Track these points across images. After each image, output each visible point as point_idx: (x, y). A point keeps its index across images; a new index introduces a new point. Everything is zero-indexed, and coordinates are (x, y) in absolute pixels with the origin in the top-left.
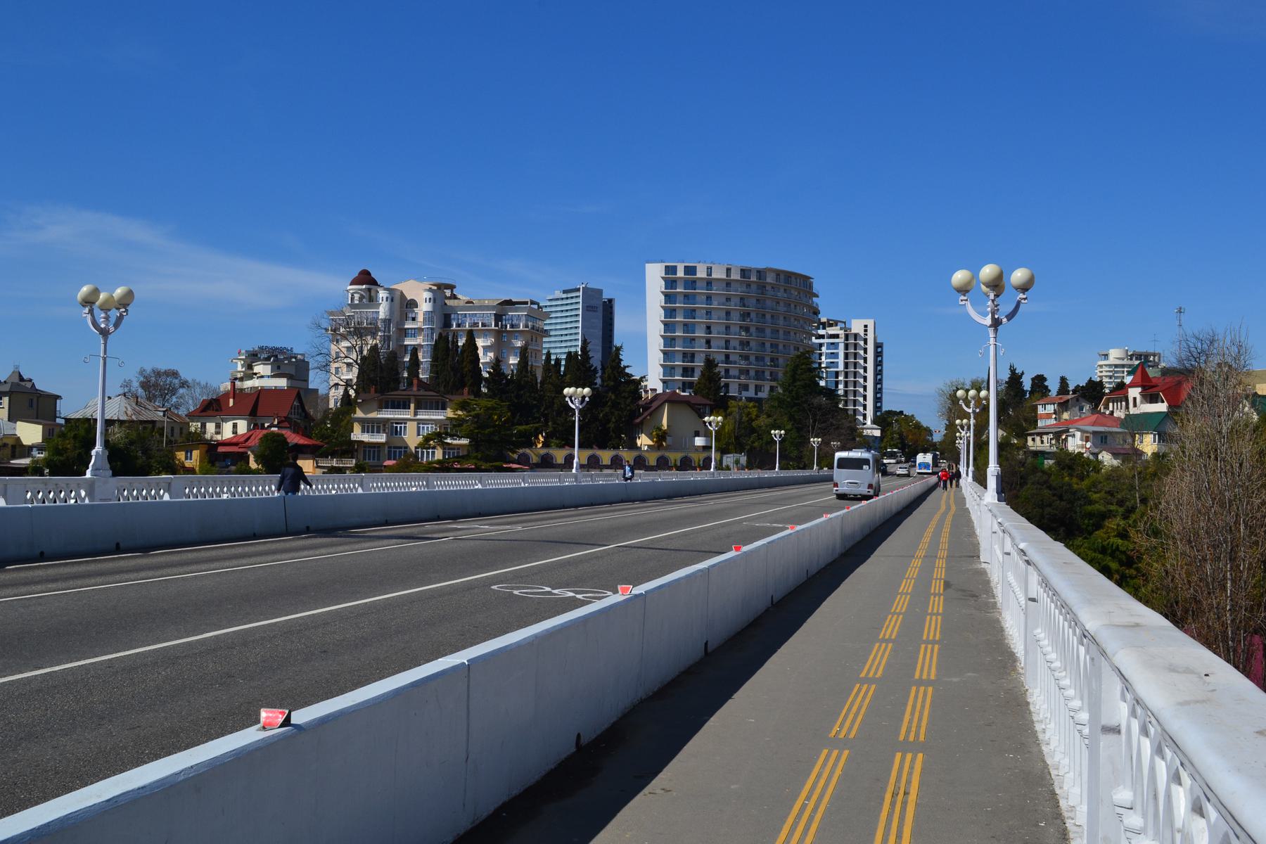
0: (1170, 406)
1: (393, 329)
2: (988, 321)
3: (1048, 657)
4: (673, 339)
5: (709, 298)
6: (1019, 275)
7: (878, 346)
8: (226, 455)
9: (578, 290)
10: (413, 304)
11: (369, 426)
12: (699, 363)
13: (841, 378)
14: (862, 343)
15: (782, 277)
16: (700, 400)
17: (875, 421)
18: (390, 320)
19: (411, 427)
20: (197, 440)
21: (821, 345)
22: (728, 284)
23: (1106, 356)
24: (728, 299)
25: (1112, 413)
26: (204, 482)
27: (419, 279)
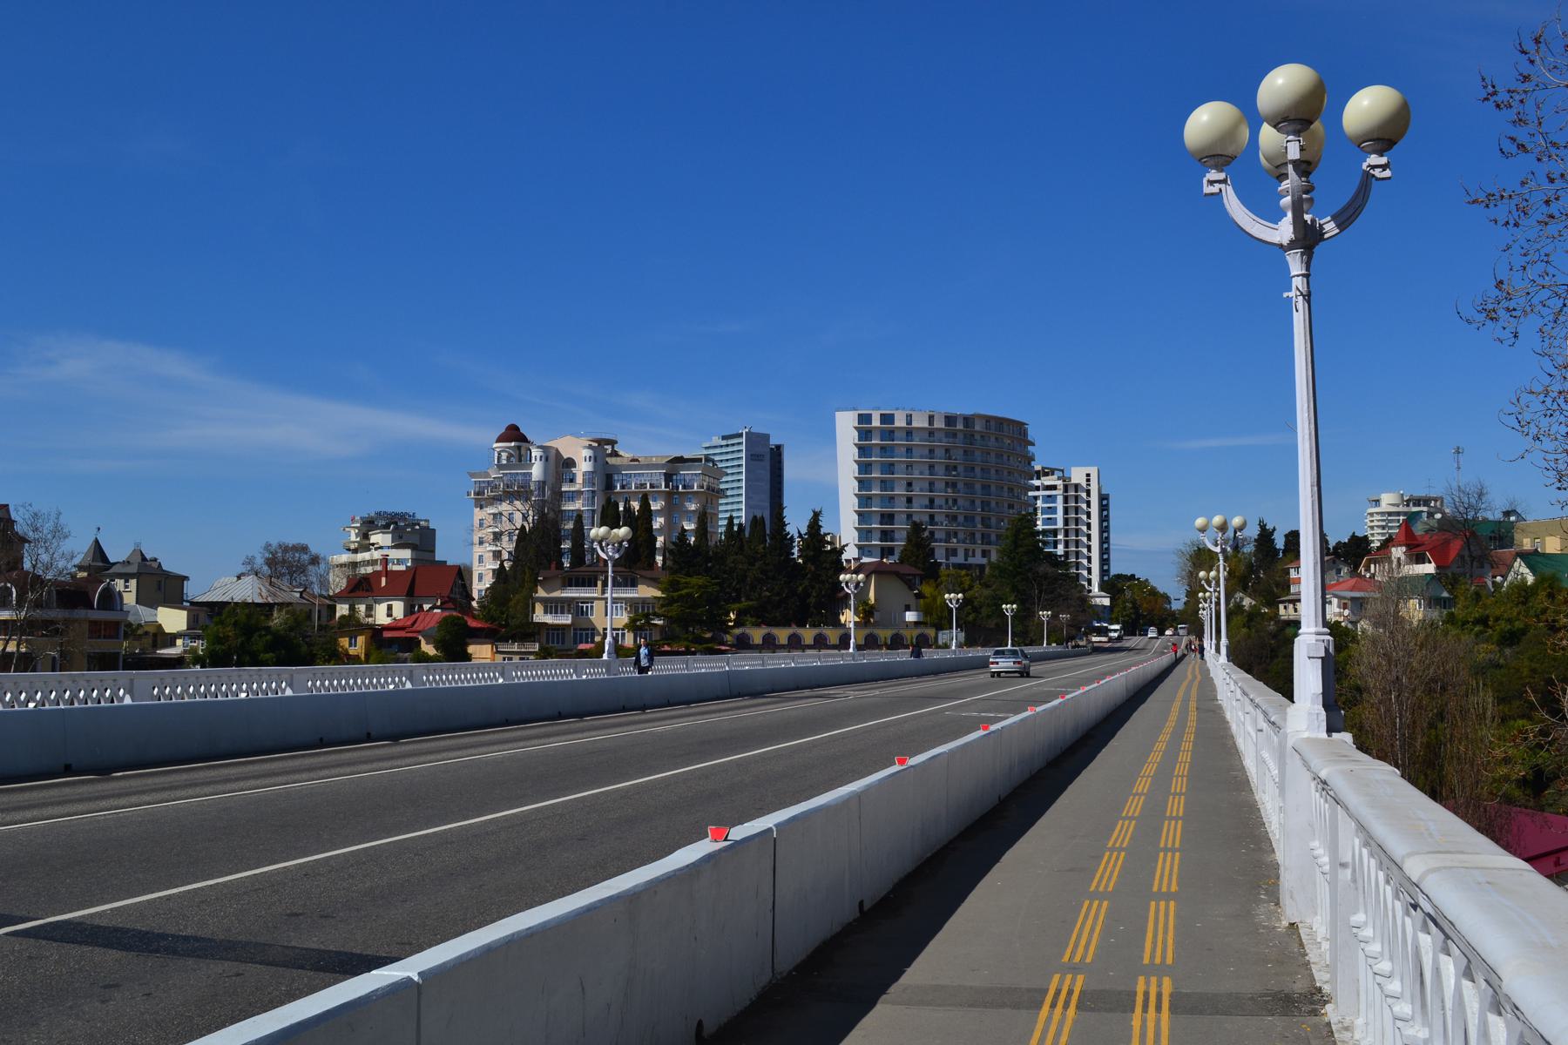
0: (1438, 567)
1: (548, 493)
2: (1284, 231)
3: (1377, 968)
4: (869, 498)
5: (909, 450)
6: (1367, 105)
7: (1103, 498)
8: (392, 641)
10: (570, 463)
11: (553, 606)
12: (901, 527)
13: (1060, 537)
14: (1084, 495)
15: (993, 423)
16: (906, 569)
17: (1104, 586)
18: (544, 482)
20: (351, 626)
21: (1036, 498)
22: (931, 433)
23: (1377, 502)
24: (931, 451)
25: (1373, 575)
26: (225, 679)
27: (578, 436)
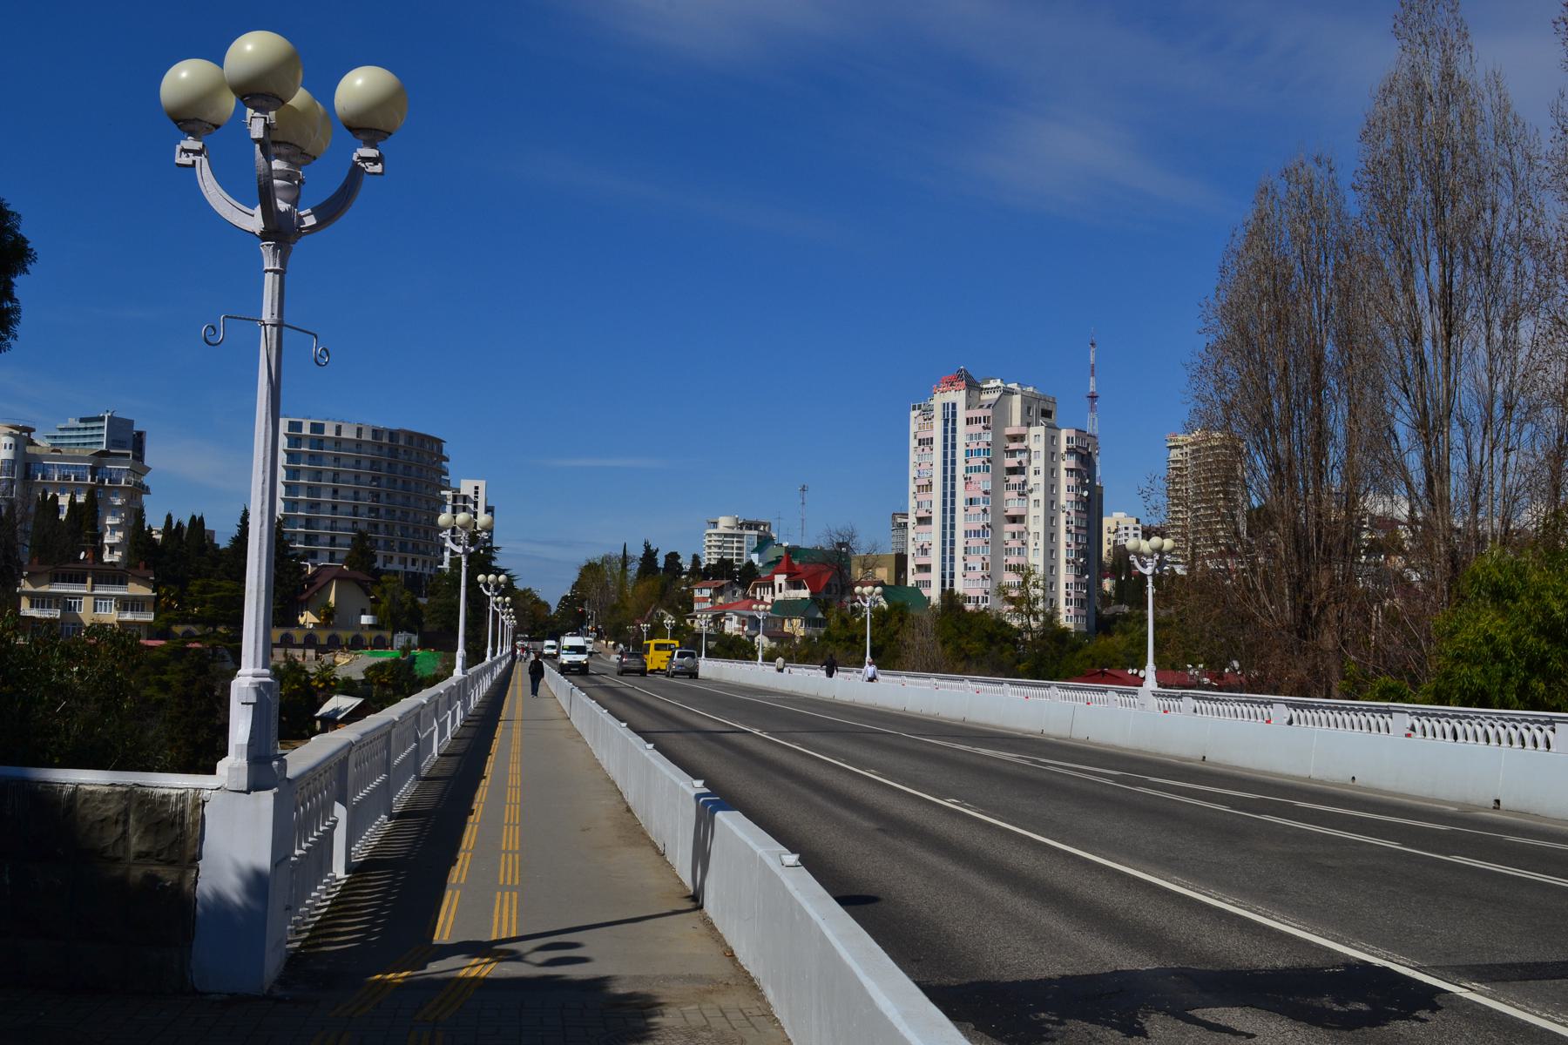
4: (296, 502)
9: (102, 419)
11: (38, 600)
19: (87, 603)
22: (359, 444)
23: (715, 524)
24: (358, 462)
